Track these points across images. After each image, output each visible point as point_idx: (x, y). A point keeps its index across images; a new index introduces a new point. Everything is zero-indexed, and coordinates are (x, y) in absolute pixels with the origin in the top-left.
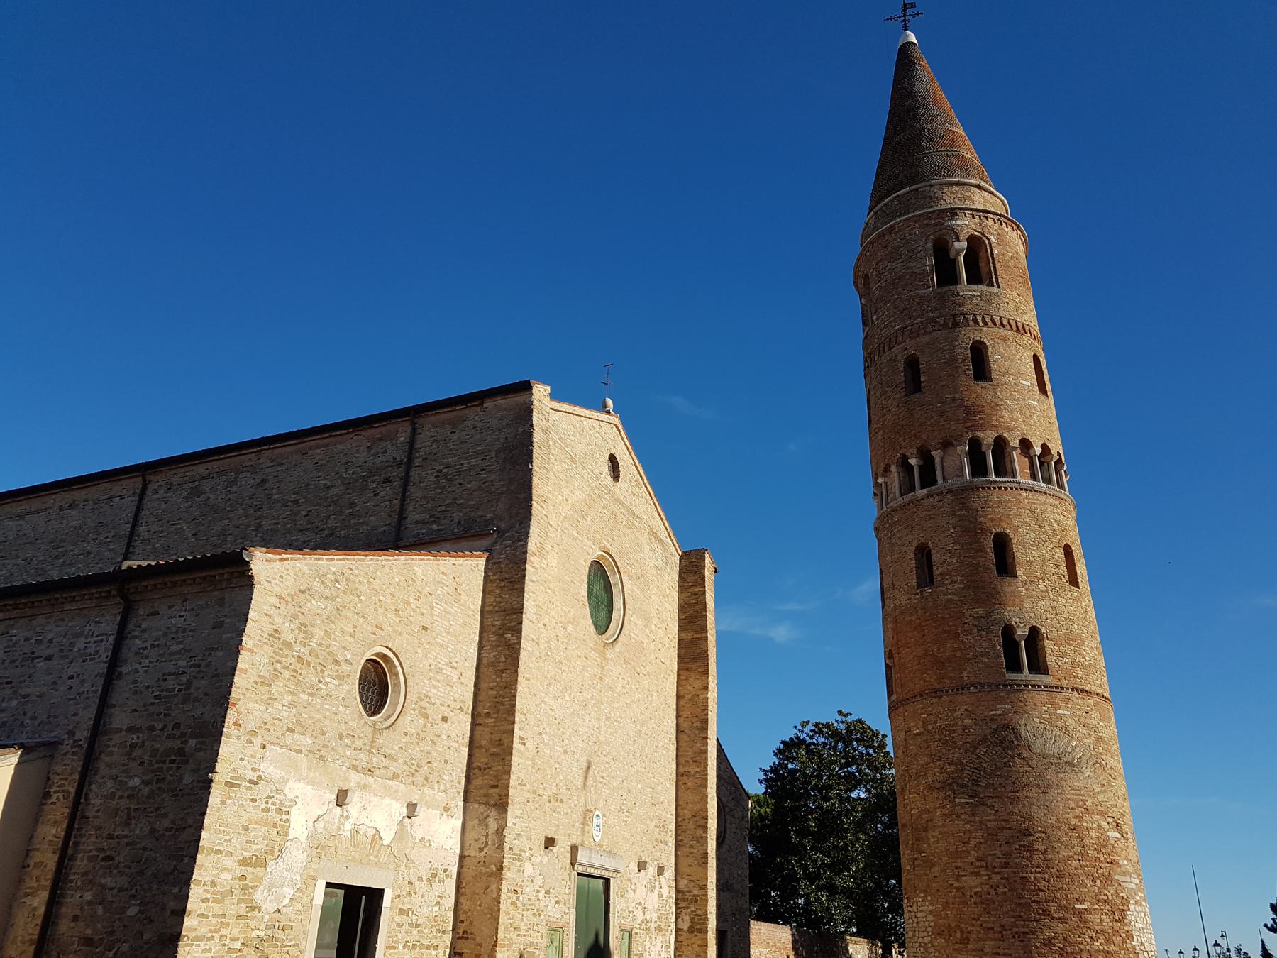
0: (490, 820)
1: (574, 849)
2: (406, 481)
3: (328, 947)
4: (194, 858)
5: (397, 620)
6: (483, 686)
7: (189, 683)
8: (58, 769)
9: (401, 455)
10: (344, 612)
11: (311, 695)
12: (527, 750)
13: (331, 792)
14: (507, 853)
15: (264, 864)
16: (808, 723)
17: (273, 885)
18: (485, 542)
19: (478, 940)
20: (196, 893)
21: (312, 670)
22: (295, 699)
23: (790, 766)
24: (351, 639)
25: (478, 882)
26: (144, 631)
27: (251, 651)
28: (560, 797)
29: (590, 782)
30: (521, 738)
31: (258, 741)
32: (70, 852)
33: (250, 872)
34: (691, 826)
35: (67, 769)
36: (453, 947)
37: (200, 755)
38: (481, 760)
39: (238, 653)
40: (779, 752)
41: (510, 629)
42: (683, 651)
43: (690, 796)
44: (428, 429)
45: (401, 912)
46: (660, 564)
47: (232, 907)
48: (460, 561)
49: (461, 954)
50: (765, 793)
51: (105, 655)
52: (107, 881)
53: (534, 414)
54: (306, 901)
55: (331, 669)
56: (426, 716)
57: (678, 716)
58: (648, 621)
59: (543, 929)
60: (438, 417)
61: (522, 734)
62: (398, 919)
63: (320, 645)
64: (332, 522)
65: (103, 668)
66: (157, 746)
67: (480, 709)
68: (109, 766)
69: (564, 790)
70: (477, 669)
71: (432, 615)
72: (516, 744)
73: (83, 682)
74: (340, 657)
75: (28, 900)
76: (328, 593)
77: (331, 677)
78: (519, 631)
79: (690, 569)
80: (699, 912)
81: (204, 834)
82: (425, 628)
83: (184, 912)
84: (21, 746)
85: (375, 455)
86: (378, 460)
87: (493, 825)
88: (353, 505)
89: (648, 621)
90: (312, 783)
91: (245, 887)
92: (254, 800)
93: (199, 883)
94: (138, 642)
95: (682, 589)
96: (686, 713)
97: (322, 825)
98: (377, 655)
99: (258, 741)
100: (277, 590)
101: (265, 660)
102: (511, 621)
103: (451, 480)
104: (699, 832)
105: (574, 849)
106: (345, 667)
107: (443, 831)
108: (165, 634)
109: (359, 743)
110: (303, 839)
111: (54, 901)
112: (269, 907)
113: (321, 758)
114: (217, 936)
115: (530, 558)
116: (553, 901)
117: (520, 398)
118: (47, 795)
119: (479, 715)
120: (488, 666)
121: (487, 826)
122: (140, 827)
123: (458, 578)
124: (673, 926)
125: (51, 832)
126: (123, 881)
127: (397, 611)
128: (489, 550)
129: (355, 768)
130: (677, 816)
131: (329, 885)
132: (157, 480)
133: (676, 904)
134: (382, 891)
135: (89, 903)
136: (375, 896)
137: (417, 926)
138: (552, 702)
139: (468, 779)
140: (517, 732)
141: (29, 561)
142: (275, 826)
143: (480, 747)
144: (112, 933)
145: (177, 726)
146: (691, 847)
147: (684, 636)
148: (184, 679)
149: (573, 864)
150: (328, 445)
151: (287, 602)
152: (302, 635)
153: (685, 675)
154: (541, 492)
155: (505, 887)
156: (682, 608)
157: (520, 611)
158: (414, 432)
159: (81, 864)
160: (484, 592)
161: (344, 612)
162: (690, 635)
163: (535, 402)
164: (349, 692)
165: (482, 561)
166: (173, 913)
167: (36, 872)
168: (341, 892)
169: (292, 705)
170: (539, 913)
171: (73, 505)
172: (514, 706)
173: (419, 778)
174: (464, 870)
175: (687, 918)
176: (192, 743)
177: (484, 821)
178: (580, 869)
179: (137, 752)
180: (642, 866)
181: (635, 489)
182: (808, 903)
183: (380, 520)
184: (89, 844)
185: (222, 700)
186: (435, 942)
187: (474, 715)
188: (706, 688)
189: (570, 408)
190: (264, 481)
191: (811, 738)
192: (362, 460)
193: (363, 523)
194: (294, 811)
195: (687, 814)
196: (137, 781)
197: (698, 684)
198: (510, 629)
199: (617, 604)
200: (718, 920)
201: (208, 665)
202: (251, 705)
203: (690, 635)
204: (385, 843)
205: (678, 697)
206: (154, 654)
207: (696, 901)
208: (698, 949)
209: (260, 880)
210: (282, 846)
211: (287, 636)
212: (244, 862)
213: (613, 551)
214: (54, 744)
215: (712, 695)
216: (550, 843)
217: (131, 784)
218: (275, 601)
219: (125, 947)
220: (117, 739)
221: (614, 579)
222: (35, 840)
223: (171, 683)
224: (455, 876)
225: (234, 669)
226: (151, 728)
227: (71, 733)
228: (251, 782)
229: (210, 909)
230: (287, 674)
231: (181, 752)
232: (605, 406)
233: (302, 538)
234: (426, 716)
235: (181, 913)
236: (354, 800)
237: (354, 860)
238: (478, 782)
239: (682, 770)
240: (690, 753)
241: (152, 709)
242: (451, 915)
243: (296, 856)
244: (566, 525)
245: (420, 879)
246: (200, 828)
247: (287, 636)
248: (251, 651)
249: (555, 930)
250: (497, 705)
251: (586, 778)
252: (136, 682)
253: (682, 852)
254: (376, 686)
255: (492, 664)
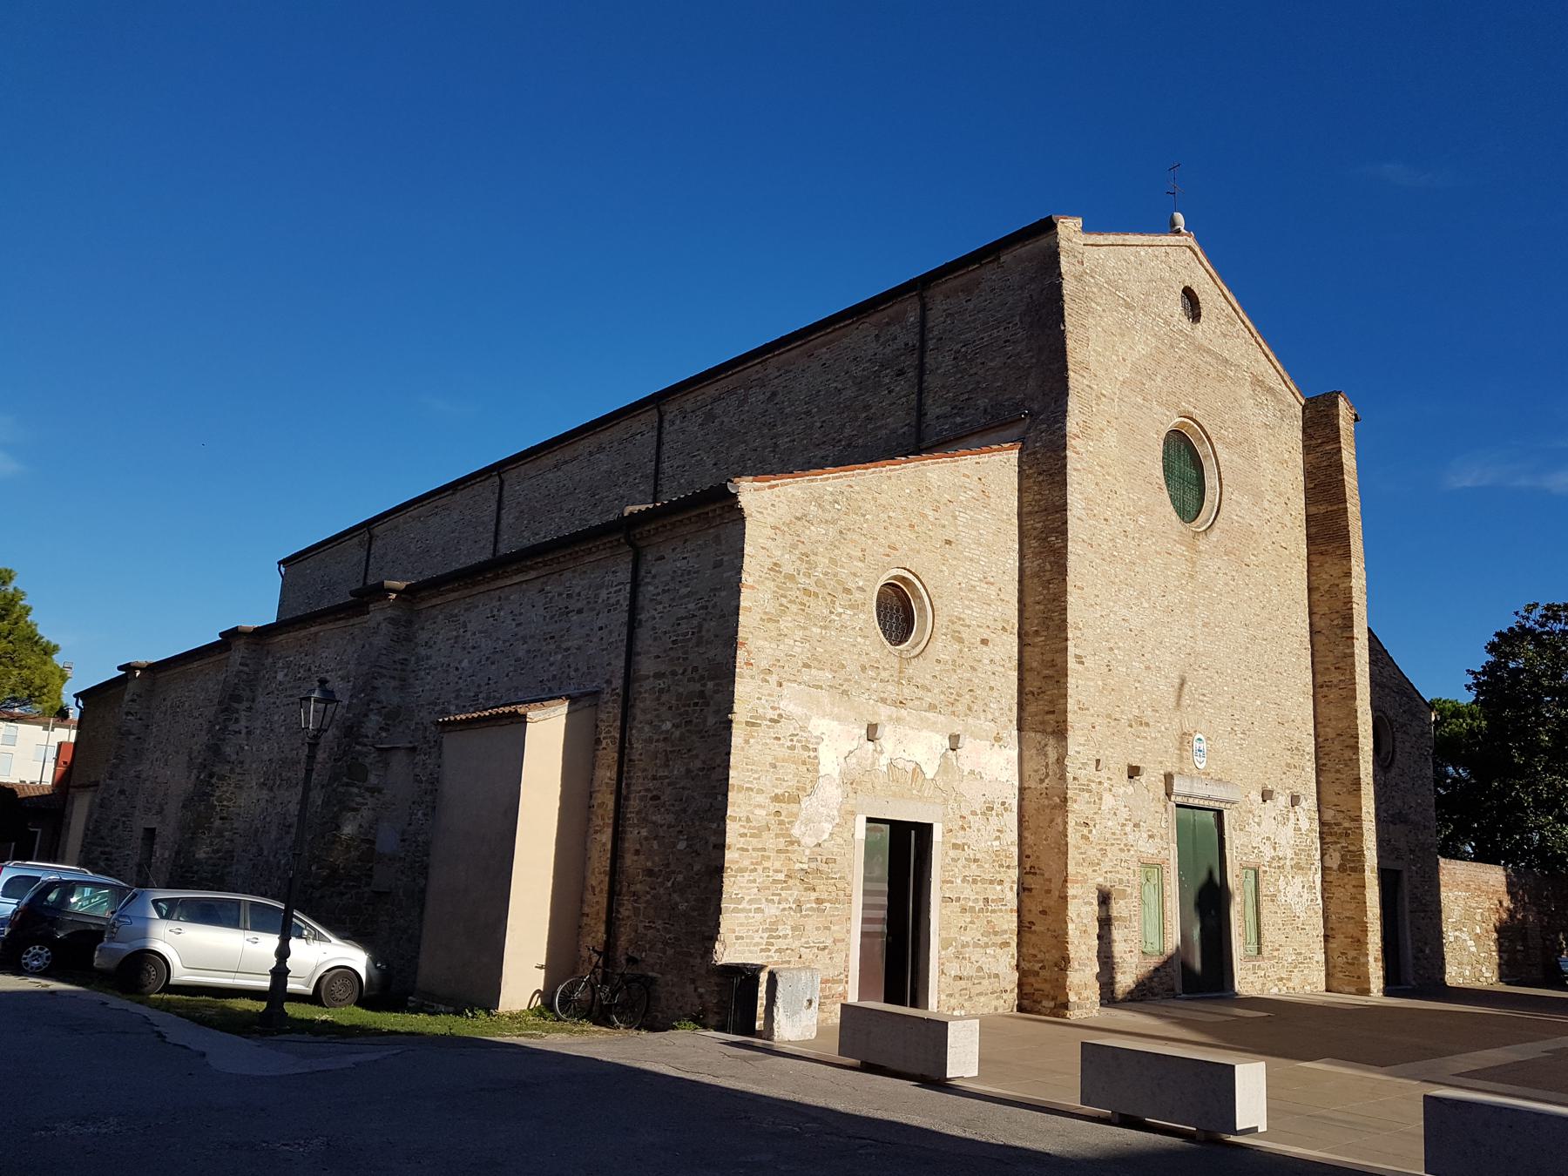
0: (1049, 749)
1: (1169, 778)
2: (921, 369)
3: (878, 880)
4: (726, 796)
5: (913, 536)
6: (1029, 600)
7: (700, 626)
8: (603, 716)
9: (913, 340)
10: (849, 535)
11: (825, 628)
12: (1087, 669)
13: (860, 727)
14: (1071, 784)
15: (796, 800)
16: (1536, 605)
17: (809, 821)
18: (1016, 431)
19: (1047, 875)
20: (732, 830)
21: (821, 602)
22: (808, 633)
23: (1512, 665)
24: (860, 564)
25: (1042, 816)
26: (654, 577)
27: (753, 588)
28: (1144, 720)
29: (1186, 701)
30: (1077, 656)
31: (773, 679)
32: (624, 792)
33: (784, 807)
34: (1337, 747)
35: (610, 713)
36: (1020, 883)
37: (718, 697)
38: (1033, 684)
39: (739, 592)
40: (1492, 648)
41: (1054, 530)
42: (1313, 530)
43: (1332, 711)
44: (940, 303)
45: (955, 846)
46: (1271, 420)
47: (771, 841)
48: (985, 458)
49: (1030, 890)
50: (1475, 702)
51: (625, 604)
52: (657, 818)
53: (1062, 258)
54: (847, 835)
55: (842, 598)
56: (961, 640)
57: (1311, 614)
58: (1257, 496)
59: (1135, 866)
60: (949, 285)
61: (1078, 652)
62: (952, 853)
63: (826, 574)
64: (847, 431)
65: (625, 617)
66: (681, 690)
67: (1027, 627)
68: (644, 711)
69: (1149, 712)
70: (1020, 582)
71: (956, 526)
72: (1072, 664)
73: (611, 632)
74: (851, 585)
75: (597, 836)
76: (828, 516)
77: (844, 607)
78: (1065, 532)
79: (1318, 425)
80: (1351, 848)
81: (732, 773)
82: (948, 542)
83: (724, 846)
84: (568, 697)
85: (884, 344)
86: (888, 350)
87: (1052, 755)
88: (867, 407)
89: (1257, 496)
90: (838, 718)
91: (781, 823)
92: (778, 739)
93: (734, 819)
94: (651, 588)
95: (1307, 449)
96: (1323, 609)
97: (854, 760)
98: (895, 578)
99: (773, 679)
100: (770, 520)
101: (768, 596)
102: (1054, 521)
103: (972, 360)
104: (1348, 754)
105: (1169, 778)
106: (858, 595)
107: (996, 764)
108: (673, 579)
109: (884, 675)
110: (836, 774)
111: (617, 837)
112: (809, 841)
113: (845, 692)
114: (760, 868)
115: (1071, 442)
116: (1145, 836)
117: (1043, 242)
118: (598, 742)
119: (1027, 634)
120: (1032, 577)
121: (1046, 755)
122: (678, 769)
123: (989, 477)
124: (1318, 864)
125: (606, 774)
126: (670, 818)
127: (912, 526)
128: (1022, 439)
129: (884, 701)
130: (1317, 736)
131: (869, 820)
132: (671, 410)
133: (1321, 838)
134: (931, 826)
135: (646, 838)
136: (925, 830)
137: (976, 861)
138: (1124, 611)
139: (1021, 706)
140: (1072, 650)
141: (572, 512)
142: (804, 763)
143: (1031, 669)
144: (668, 865)
145: (695, 669)
146: (1338, 771)
147: (1313, 510)
148: (695, 622)
149: (1168, 795)
150: (832, 341)
151: (784, 532)
152: (805, 565)
153: (1317, 560)
154: (1079, 358)
155: (1072, 820)
156: (1309, 474)
157: (1063, 508)
158: (924, 308)
159: (634, 804)
160: (1020, 490)
161: (849, 535)
162: (1322, 509)
163: (1063, 243)
164: (866, 621)
165: (1014, 455)
166: (715, 846)
167: (600, 812)
168: (886, 827)
169: (805, 640)
170: (1128, 847)
171: (601, 449)
172: (1065, 620)
173: (960, 707)
174: (1025, 803)
175: (1337, 855)
176: (710, 685)
177: (1042, 751)
178: (1180, 800)
179: (664, 698)
180: (1266, 795)
181: (1228, 331)
182: (1543, 838)
183: (898, 422)
184: (638, 785)
185: (730, 641)
186: (999, 877)
187: (1021, 635)
188: (1348, 574)
189: (1119, 239)
190: (774, 394)
191: (1542, 625)
192: (871, 352)
193: (880, 428)
194: (821, 748)
195: (1331, 733)
196: (668, 725)
197: (1336, 571)
198: (1054, 530)
199: (1211, 481)
200: (1380, 857)
201: (714, 607)
202: (761, 643)
203: (1322, 509)
204: (929, 776)
205: (1310, 590)
206: (665, 598)
207: (1347, 835)
208: (1353, 890)
209: (796, 815)
210: (814, 782)
211: (788, 568)
212: (776, 798)
213: (1197, 414)
214: (596, 694)
215: (1358, 582)
216: (1134, 772)
217: (664, 728)
218: (770, 532)
219: (680, 878)
220: (647, 685)
221: (1203, 450)
222: (596, 784)
223: (684, 626)
224: (1015, 809)
225: (738, 607)
226: (674, 673)
227: (609, 682)
228: (772, 720)
229: (749, 843)
230: (794, 608)
231: (702, 694)
232: (1173, 223)
233: (821, 453)
234: (961, 640)
235: (721, 847)
236: (886, 734)
237: (894, 795)
238: (1031, 708)
239: (1320, 680)
240: (1330, 659)
241: (672, 654)
242: (1015, 850)
243: (831, 792)
244: (1126, 391)
245: (974, 813)
246: (728, 767)
247: (788, 568)
248: (753, 588)
249: (1151, 867)
250: (1046, 620)
251: (1179, 697)
252: (654, 628)
253: (1327, 777)
254: (898, 612)
255: (1036, 575)
